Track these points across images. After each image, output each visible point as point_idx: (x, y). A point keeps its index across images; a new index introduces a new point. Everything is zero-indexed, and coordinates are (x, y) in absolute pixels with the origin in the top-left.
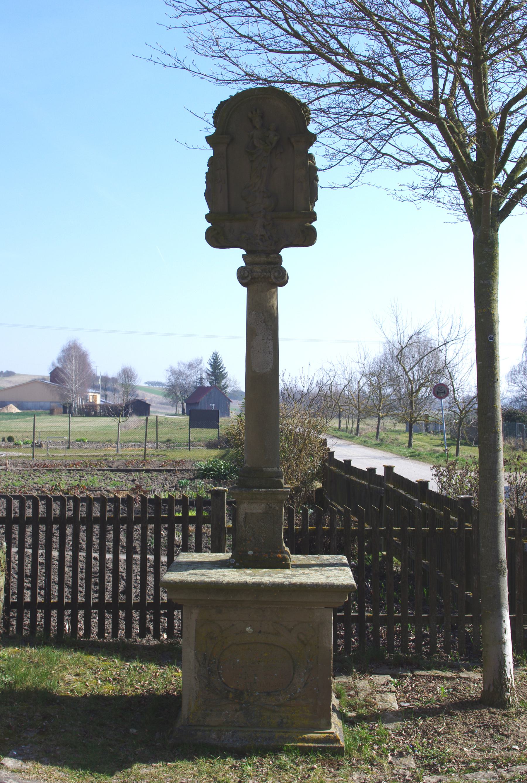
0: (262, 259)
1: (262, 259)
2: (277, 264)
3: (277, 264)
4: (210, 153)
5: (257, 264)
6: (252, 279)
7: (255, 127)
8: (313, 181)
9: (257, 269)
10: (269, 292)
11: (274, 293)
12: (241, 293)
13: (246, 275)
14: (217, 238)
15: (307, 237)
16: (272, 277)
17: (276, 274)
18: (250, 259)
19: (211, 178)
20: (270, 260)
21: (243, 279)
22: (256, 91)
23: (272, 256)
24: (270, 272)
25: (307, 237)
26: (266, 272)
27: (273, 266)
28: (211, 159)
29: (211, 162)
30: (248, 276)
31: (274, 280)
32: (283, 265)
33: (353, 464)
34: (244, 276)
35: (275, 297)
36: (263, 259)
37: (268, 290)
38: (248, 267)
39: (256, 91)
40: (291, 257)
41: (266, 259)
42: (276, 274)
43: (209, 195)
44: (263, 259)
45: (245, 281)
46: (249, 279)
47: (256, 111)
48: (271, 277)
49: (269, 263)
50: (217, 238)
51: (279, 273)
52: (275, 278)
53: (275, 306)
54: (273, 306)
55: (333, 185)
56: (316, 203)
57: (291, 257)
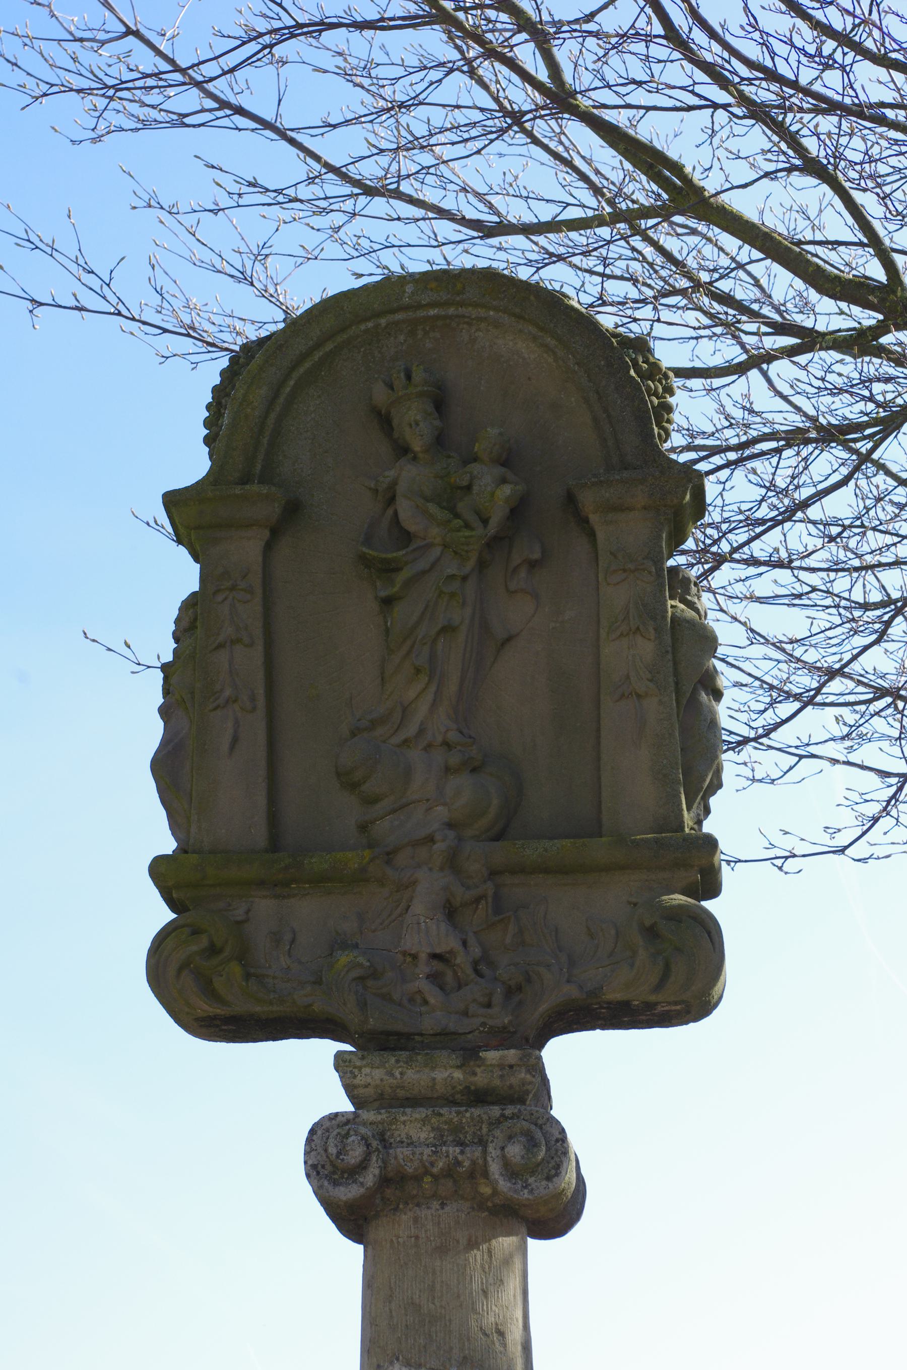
0: (440, 1075)
1: (440, 1075)
2: (522, 1101)
3: (522, 1101)
4: (183, 575)
5: (413, 1102)
6: (385, 1181)
7: (403, 450)
8: (693, 700)
9: (413, 1127)
10: (477, 1256)
11: (507, 1262)
12: (340, 1264)
13: (355, 1154)
14: (215, 980)
15: (672, 977)
16: (495, 1168)
17: (515, 1151)
18: (378, 1074)
19: (188, 687)
20: (481, 1079)
21: (336, 1183)
22: (409, 288)
23: (491, 1056)
24: (482, 1142)
25: (672, 977)
26: (461, 1144)
27: (496, 1111)
28: (191, 605)
29: (193, 619)
30: (363, 1166)
31: (503, 1185)
32: (556, 1112)
33: (193, 464)
34: (355, 1178)
35: (513, 1284)
36: (446, 1073)
37: (472, 1244)
38: (369, 1115)
39: (409, 288)
40: (596, 1081)
41: (458, 1075)
42: (515, 1151)
43: (171, 770)
44: (446, 1073)
45: (347, 1193)
46: (370, 1178)
47: (409, 377)
48: (486, 1174)
49: (479, 1097)
50: (215, 980)
51: (532, 1144)
52: (512, 1172)
53: (515, 1334)
54: (501, 1334)
55: (787, 844)
56: (713, 801)
57: (596, 1081)
